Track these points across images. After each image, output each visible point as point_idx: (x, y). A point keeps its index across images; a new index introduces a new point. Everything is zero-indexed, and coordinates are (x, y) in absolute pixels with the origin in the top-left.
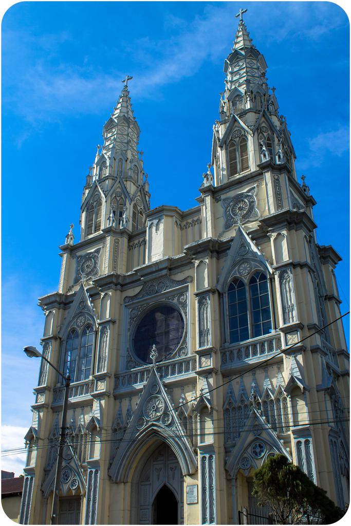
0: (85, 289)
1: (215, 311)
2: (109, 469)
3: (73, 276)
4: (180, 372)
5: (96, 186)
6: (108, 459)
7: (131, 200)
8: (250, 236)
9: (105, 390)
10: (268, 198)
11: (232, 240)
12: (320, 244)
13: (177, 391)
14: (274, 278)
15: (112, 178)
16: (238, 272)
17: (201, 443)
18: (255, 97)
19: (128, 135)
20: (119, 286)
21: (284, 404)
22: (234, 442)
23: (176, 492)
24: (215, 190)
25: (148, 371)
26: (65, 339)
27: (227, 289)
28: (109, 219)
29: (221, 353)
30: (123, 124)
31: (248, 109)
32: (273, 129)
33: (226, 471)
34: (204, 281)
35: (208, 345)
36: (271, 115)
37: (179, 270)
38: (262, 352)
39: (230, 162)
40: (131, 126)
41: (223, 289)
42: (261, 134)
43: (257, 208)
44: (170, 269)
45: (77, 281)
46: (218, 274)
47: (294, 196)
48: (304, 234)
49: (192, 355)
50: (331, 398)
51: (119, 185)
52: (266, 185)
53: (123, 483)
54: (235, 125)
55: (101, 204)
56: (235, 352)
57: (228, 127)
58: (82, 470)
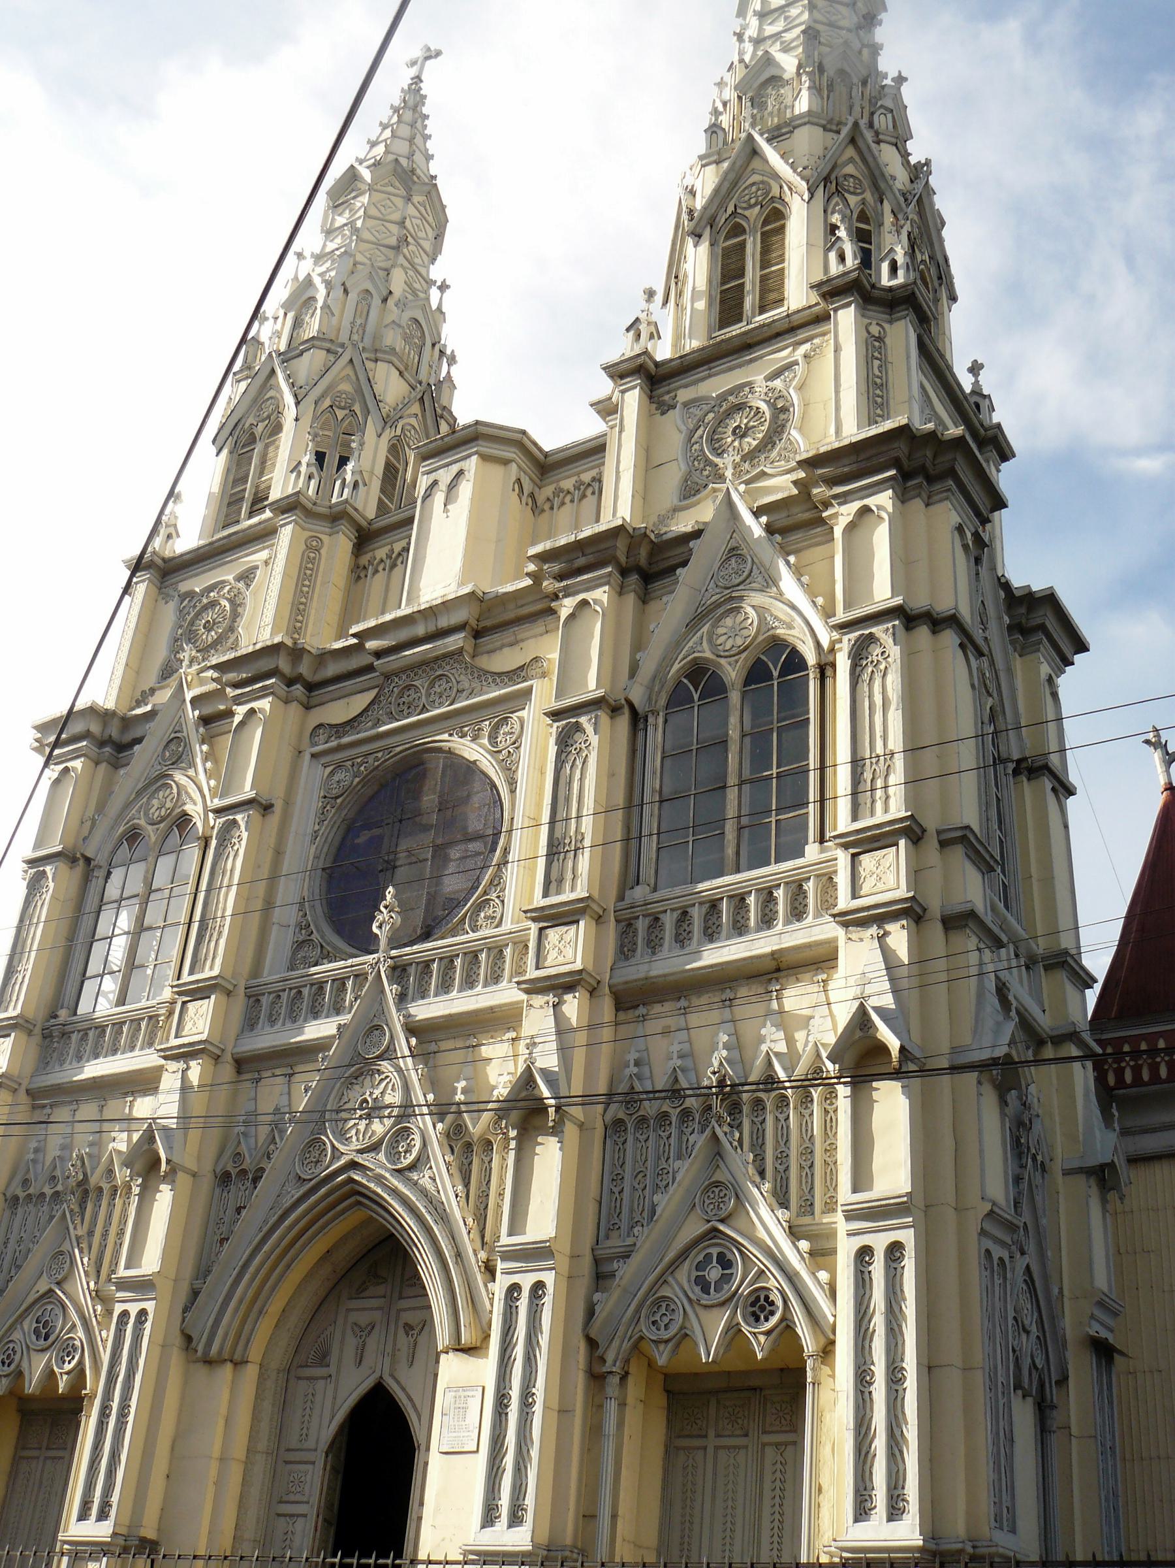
0: (189, 696)
1: (612, 775)
2: (186, 1310)
3: (161, 653)
4: (469, 982)
5: (273, 371)
6: (188, 1271)
7: (387, 421)
8: (764, 519)
9: (204, 1037)
10: (837, 392)
11: (697, 534)
12: (1017, 581)
13: (451, 1054)
14: (833, 665)
15: (328, 345)
16: (710, 641)
17: (511, 1234)
18: (831, 87)
19: (402, 223)
20: (298, 690)
21: (826, 1112)
22: (629, 1241)
23: (416, 1410)
24: (662, 371)
25: (360, 977)
26: (104, 863)
27: (662, 702)
28: (296, 468)
29: (618, 921)
30: (390, 189)
31: (801, 116)
32: (883, 185)
33: (592, 1343)
34: (589, 667)
35: (573, 890)
36: (878, 142)
37: (507, 636)
38: (767, 920)
39: (723, 284)
40: (416, 199)
41: (650, 699)
42: (836, 199)
43: (800, 429)
44: (477, 634)
45: (168, 671)
46: (638, 645)
47: (933, 409)
48: (955, 519)
49: (515, 927)
50: (1003, 1102)
51: (349, 371)
52: (837, 350)
53: (229, 1367)
54: (750, 168)
55: (278, 428)
56: (669, 920)
57: (726, 173)
58: (99, 1308)
